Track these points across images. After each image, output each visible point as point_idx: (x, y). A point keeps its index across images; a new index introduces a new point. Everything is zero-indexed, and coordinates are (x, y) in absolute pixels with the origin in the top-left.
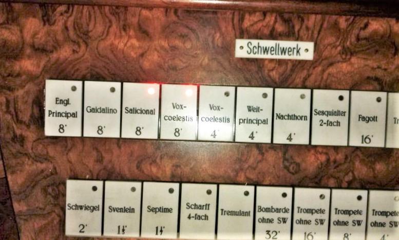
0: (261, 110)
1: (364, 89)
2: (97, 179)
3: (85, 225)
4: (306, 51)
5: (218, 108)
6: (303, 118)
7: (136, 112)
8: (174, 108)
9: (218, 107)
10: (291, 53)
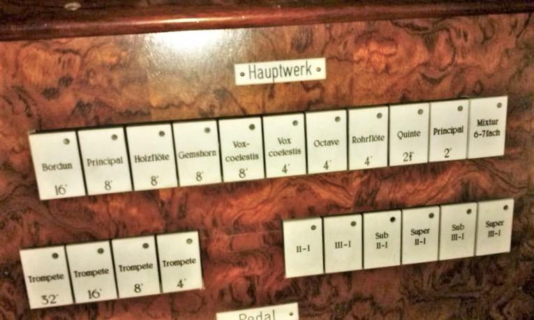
0: (248, 144)
1: (314, 108)
2: (104, 240)
3: (55, 294)
4: (315, 69)
5: (244, 145)
6: (211, 154)
7: (204, 154)
8: (280, 143)
9: (244, 143)
10: (300, 72)
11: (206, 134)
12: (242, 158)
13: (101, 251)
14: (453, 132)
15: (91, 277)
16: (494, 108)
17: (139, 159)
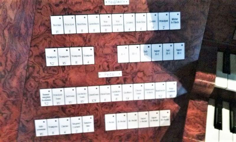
5: (106, 22)
12: (106, 26)
14: (71, 25)
17: (78, 24)
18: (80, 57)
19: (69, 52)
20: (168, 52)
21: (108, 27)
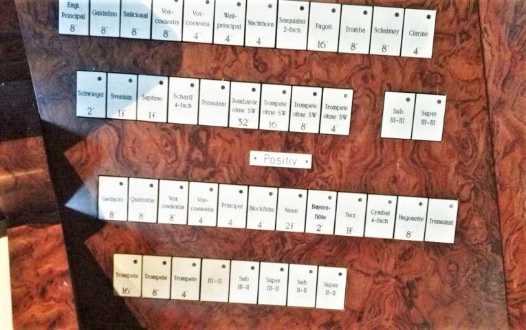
11: (300, 198)
12: (202, 210)
13: (340, 274)
15: (184, 282)
16: (447, 209)
17: (402, 218)
18: (194, 282)
19: (141, 266)
20: (244, 284)
21: (178, 210)
